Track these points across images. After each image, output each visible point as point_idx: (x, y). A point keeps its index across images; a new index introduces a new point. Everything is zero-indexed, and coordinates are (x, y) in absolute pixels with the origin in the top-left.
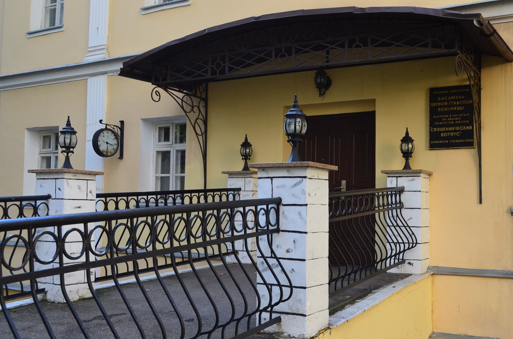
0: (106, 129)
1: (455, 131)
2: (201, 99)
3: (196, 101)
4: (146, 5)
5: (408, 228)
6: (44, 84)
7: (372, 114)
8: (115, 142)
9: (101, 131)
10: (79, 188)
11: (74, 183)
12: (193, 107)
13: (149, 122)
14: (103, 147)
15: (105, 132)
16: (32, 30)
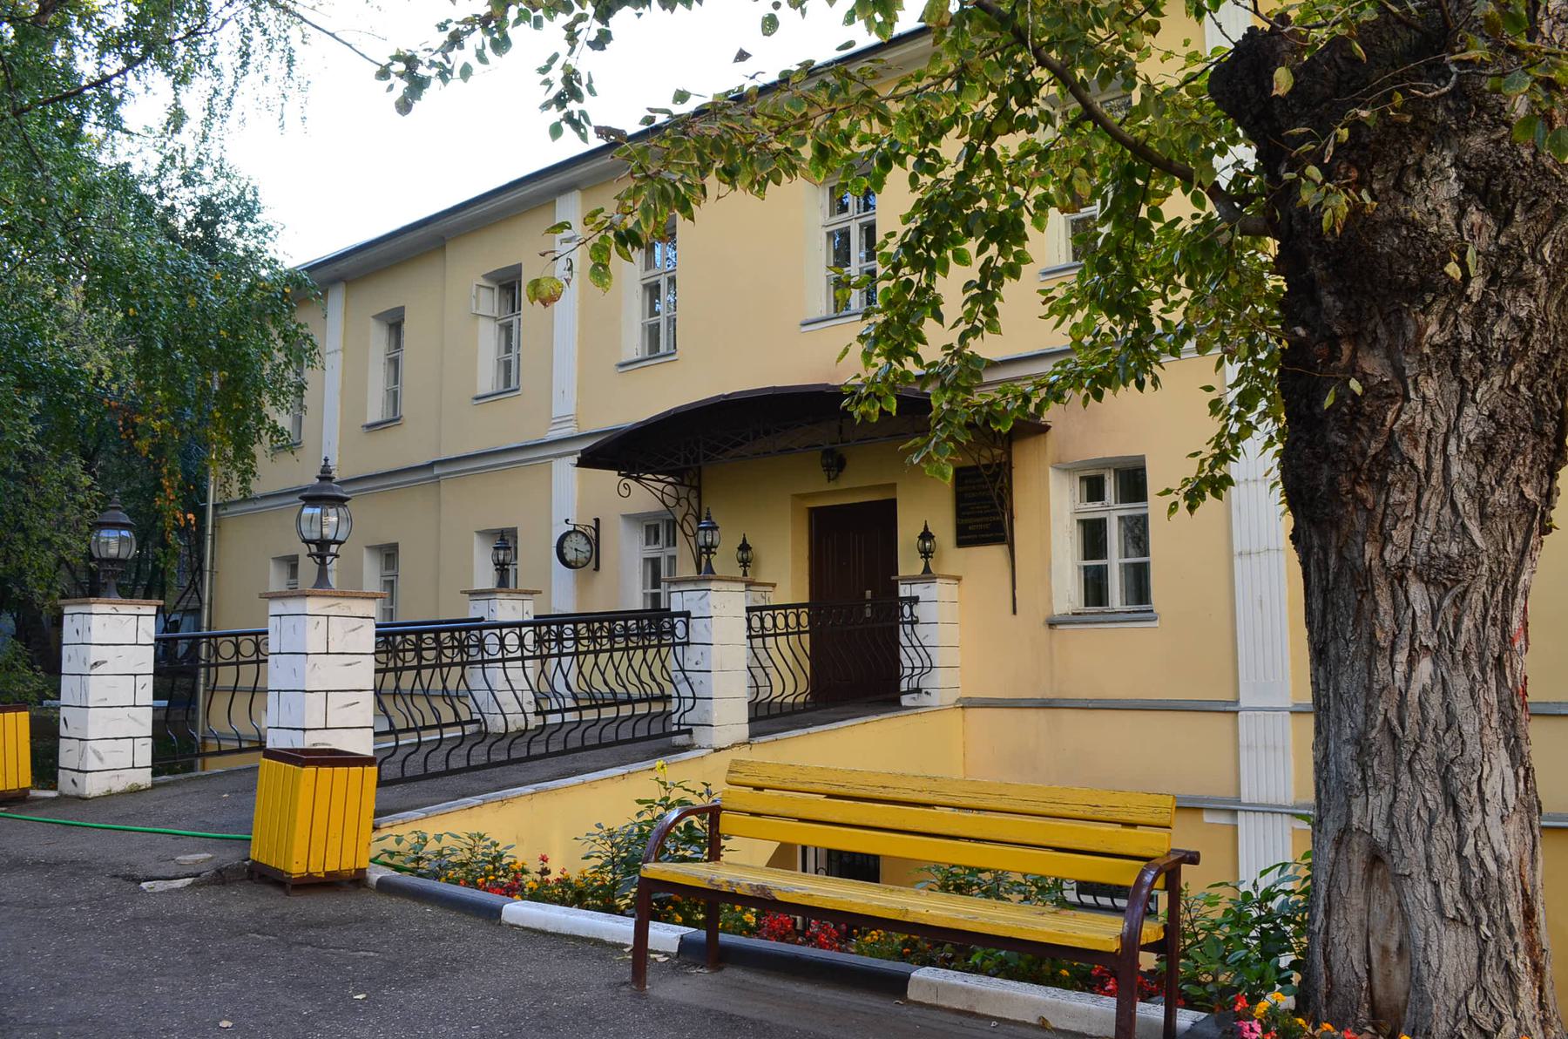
0: (575, 531)
1: (984, 523)
2: (692, 487)
3: (683, 491)
4: (624, 360)
5: (920, 650)
6: (506, 460)
7: (892, 505)
8: (588, 547)
9: (568, 533)
10: (514, 609)
11: (508, 604)
12: (678, 499)
13: (630, 518)
14: (570, 556)
15: (573, 536)
16: (480, 393)
